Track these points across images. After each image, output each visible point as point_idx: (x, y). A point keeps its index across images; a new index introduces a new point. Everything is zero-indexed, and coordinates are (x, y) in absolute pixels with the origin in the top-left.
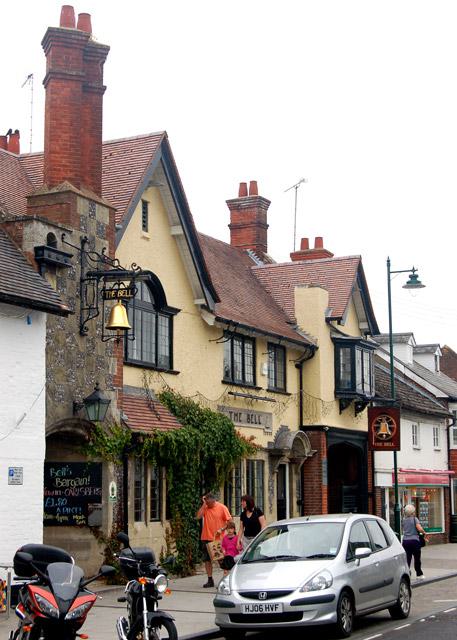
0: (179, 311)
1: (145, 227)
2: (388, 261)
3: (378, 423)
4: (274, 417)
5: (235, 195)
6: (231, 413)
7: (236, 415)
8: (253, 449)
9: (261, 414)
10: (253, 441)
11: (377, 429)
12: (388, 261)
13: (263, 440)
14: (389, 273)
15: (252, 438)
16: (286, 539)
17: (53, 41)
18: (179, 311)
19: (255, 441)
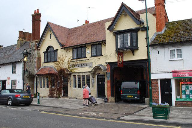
3: (120, 57)
5: (36, 10)
9: (86, 64)
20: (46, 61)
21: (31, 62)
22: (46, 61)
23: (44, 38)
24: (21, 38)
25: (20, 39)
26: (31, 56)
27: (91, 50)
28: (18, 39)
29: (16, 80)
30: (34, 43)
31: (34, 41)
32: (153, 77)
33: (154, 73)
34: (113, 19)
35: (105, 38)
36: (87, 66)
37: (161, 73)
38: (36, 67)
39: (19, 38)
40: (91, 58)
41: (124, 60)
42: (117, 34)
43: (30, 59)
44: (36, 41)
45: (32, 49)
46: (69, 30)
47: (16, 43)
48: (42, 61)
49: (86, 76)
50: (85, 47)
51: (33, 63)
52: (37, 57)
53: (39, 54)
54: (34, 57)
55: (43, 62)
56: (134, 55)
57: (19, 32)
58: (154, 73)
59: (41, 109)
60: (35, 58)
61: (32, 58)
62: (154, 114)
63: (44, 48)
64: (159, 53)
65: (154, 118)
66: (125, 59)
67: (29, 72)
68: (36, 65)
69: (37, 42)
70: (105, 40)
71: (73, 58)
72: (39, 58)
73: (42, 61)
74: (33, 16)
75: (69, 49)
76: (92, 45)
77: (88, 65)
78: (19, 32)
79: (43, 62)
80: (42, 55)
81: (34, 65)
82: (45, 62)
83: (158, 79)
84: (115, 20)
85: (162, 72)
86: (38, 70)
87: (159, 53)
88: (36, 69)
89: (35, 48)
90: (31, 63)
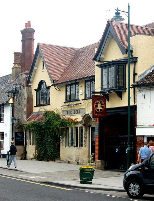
0: (35, 90)
1: (43, 68)
2: (129, 6)
3: (97, 104)
4: (86, 109)
5: (27, 23)
6: (67, 112)
7: (69, 112)
8: (75, 122)
9: (80, 110)
10: (76, 120)
11: (97, 106)
12: (129, 6)
13: (79, 118)
14: (129, 13)
15: (76, 119)
16: (71, 162)
17: (23, 32)
18: (35, 90)
19: (77, 120)
20: (38, 104)
21: (20, 104)
22: (38, 104)
23: (35, 68)
24: (17, 64)
25: (17, 66)
26: (20, 96)
27: (84, 90)
28: (12, 65)
29: (3, 132)
30: (24, 76)
31: (23, 73)
32: (139, 132)
33: (141, 127)
34: (98, 45)
35: (94, 73)
36: (80, 113)
37: (145, 127)
38: (25, 112)
39: (15, 64)
40: (84, 101)
41: (107, 107)
42: (104, 66)
43: (20, 99)
44: (25, 72)
45: (21, 85)
46: (78, 50)
47: (10, 72)
48: (34, 104)
49: (79, 128)
50: (78, 83)
51: (23, 107)
52: (26, 97)
53: (30, 93)
54: (23, 97)
55: (35, 106)
56: (122, 99)
57: (15, 53)
58: (141, 127)
59: (108, 187)
60: (25, 98)
61: (22, 99)
62: (81, 179)
63: (35, 86)
64: (145, 98)
65: (81, 183)
66: (109, 105)
67: (18, 120)
68: (25, 109)
69: (26, 74)
70: (94, 76)
71: (66, 101)
72: (30, 100)
73: (34, 104)
74: (26, 24)
75: (61, 87)
76: (86, 82)
77: (81, 111)
78: (15, 53)
79: (35, 106)
80: (34, 94)
81: (23, 110)
82: (37, 106)
83: (144, 136)
84: (102, 45)
85: (148, 126)
86: (27, 117)
87: (145, 98)
88: (25, 116)
89: (24, 83)
90: (20, 106)
